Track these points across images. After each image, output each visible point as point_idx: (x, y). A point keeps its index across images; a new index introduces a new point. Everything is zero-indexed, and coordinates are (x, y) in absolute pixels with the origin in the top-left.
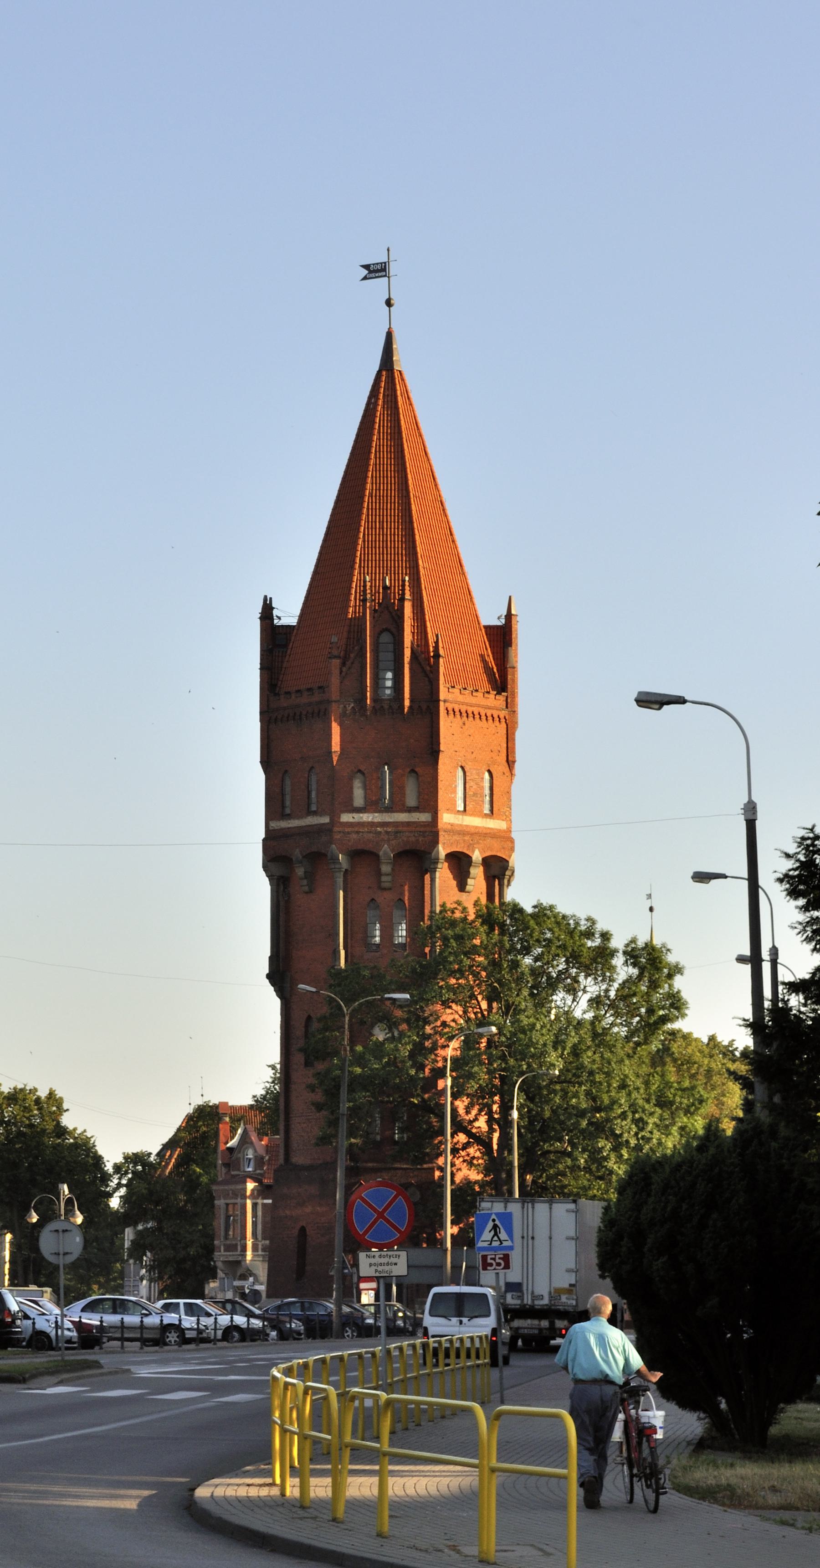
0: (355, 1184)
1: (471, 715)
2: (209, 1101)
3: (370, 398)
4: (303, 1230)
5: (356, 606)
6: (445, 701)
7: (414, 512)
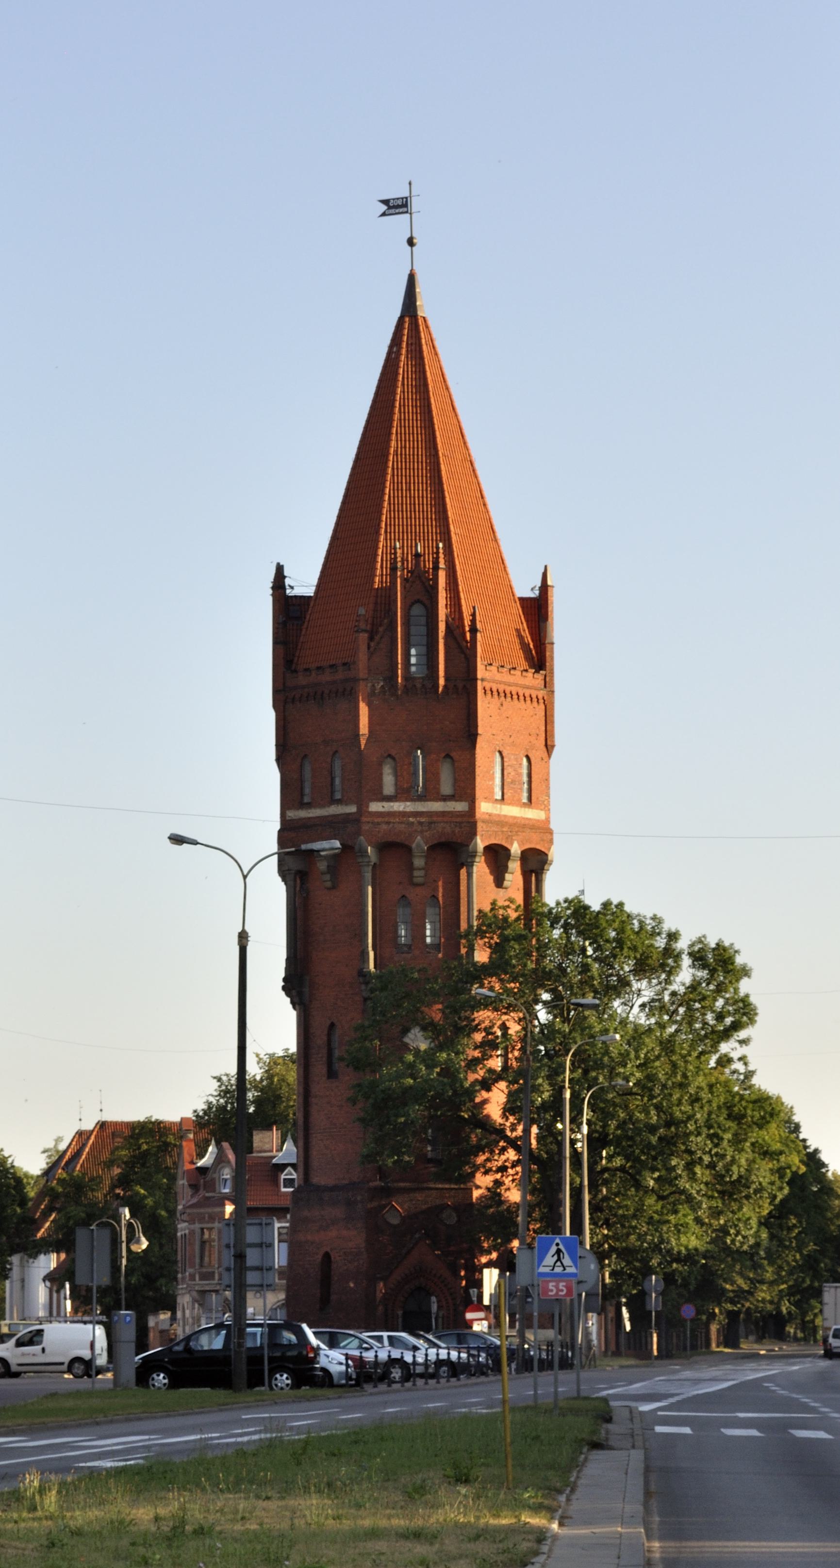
0: (385, 1206)
1: (509, 695)
2: (151, 1117)
3: (391, 347)
4: (327, 1256)
5: (382, 575)
6: (482, 680)
7: (443, 473)
